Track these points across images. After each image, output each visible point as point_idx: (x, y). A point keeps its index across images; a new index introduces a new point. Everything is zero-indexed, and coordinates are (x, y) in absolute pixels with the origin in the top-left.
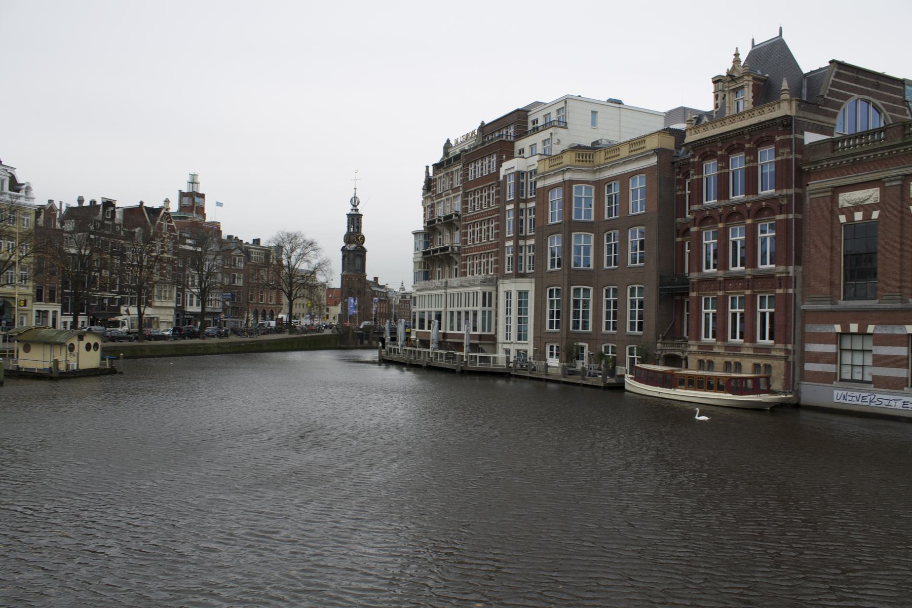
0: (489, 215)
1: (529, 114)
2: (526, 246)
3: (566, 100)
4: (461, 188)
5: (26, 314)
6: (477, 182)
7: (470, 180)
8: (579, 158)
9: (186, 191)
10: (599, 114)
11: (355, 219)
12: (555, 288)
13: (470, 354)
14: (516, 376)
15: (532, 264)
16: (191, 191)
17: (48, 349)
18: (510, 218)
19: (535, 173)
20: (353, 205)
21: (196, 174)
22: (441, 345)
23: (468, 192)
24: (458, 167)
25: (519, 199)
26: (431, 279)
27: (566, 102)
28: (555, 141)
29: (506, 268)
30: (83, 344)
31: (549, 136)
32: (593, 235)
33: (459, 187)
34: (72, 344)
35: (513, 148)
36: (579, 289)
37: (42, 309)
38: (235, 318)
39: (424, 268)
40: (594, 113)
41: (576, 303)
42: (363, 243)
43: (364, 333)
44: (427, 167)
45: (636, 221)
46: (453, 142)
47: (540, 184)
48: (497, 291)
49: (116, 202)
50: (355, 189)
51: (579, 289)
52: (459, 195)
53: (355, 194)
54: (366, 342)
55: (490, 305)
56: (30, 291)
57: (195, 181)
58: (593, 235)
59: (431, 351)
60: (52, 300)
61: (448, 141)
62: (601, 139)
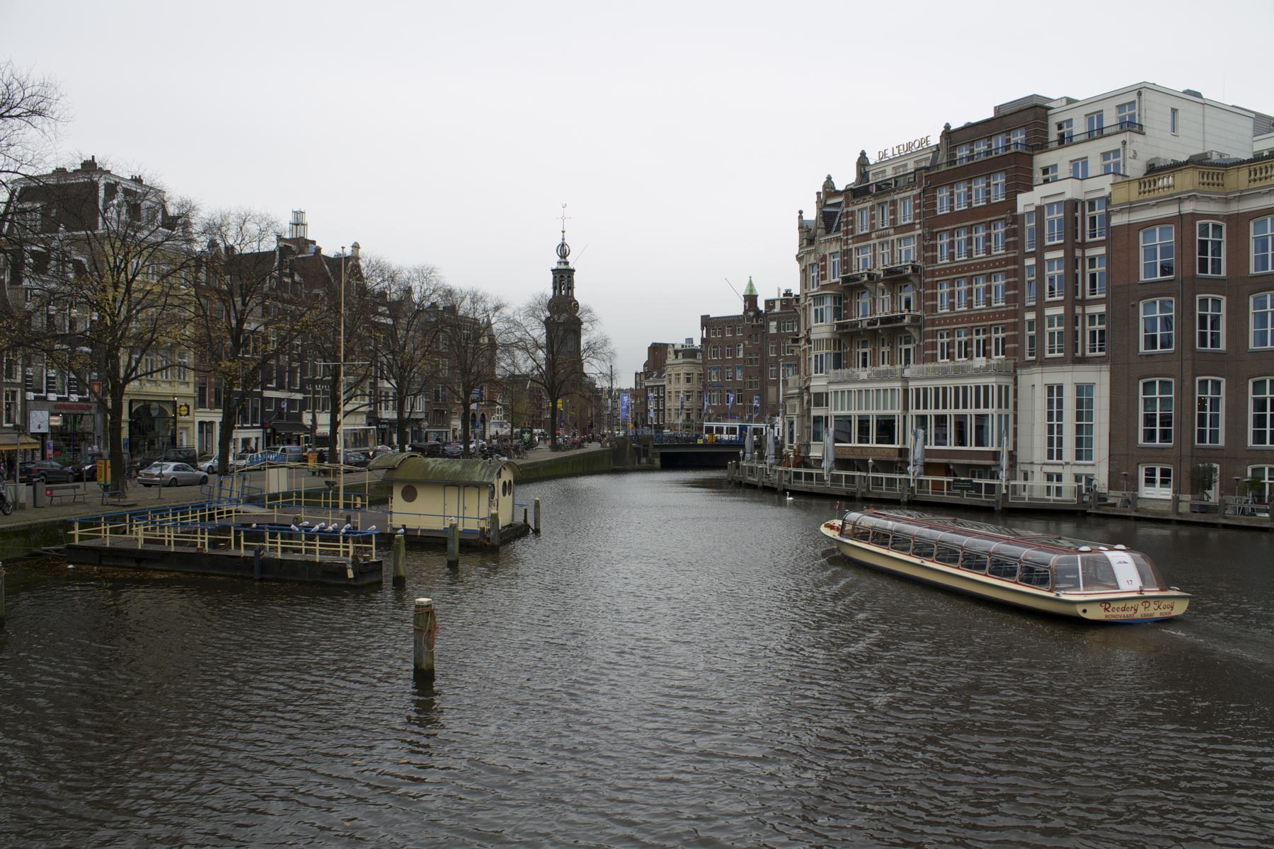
0: (972, 271)
1: (1050, 112)
3: (1140, 90)
4: (917, 226)
5: (186, 429)
6: (954, 217)
7: (939, 213)
10: (1180, 113)
11: (566, 276)
13: (836, 472)
14: (1098, 515)
17: (452, 497)
20: (561, 257)
22: (929, 468)
24: (908, 194)
25: (1073, 242)
26: (848, 366)
27: (1140, 94)
28: (1129, 154)
29: (1047, 348)
31: (1119, 146)
32: (1224, 298)
33: (914, 224)
35: (1031, 164)
36: (1206, 381)
37: (207, 420)
38: (440, 427)
39: (835, 349)
40: (1174, 111)
43: (641, 446)
46: (873, 158)
47: (1116, 221)
48: (1016, 383)
51: (1206, 381)
52: (913, 236)
54: (644, 460)
55: (1007, 407)
56: (190, 390)
57: (300, 221)
58: (1224, 298)
59: (911, 478)
61: (863, 154)
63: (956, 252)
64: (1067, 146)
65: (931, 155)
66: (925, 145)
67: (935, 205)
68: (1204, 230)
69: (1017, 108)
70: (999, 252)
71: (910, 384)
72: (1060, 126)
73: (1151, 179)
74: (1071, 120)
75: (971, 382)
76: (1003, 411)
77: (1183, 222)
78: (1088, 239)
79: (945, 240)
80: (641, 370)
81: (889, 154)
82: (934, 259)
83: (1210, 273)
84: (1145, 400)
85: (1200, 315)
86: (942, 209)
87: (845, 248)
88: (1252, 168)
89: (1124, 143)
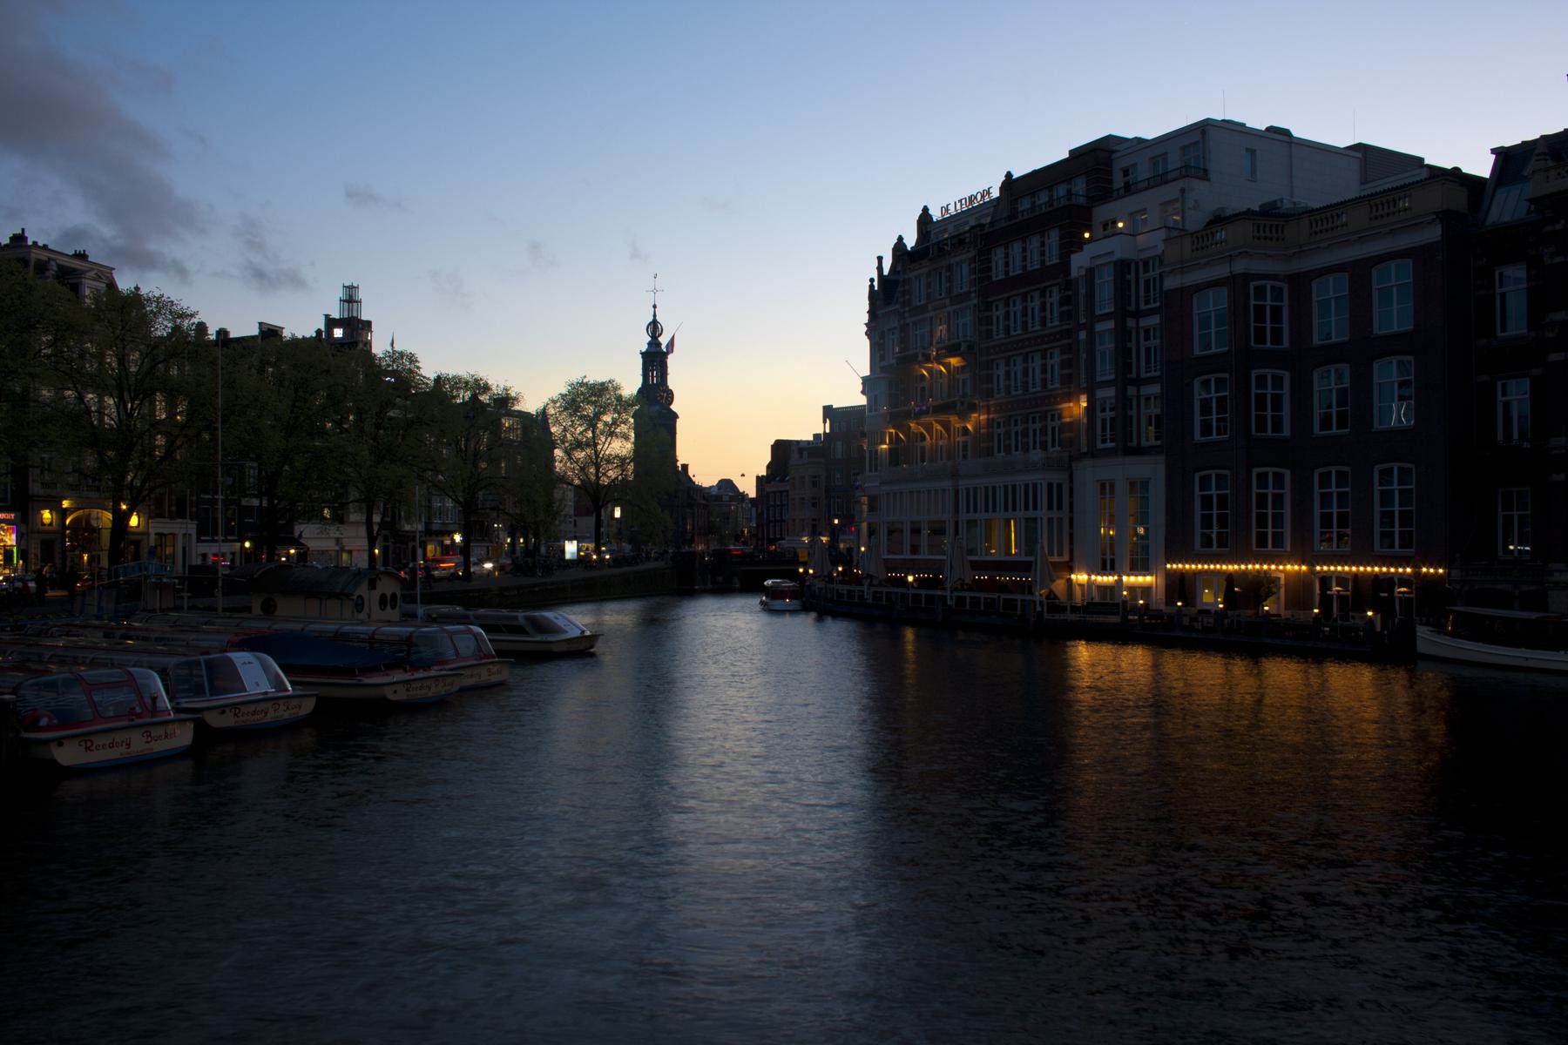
1: (1114, 156)
2: (1138, 328)
4: (973, 295)
6: (1011, 283)
7: (994, 279)
8: (1258, 232)
9: (337, 317)
12: (1213, 473)
15: (1108, 432)
16: (346, 316)
18: (1106, 346)
19: (1161, 262)
21: (355, 285)
23: (992, 302)
24: (964, 256)
25: (1125, 309)
27: (1204, 133)
30: (376, 595)
33: (970, 292)
34: (360, 597)
36: (1266, 474)
41: (1262, 499)
42: (671, 402)
44: (880, 259)
45: (1391, 345)
46: (936, 214)
47: (1169, 284)
48: (1071, 481)
49: (284, 331)
50: (655, 307)
53: (655, 316)
55: (1060, 507)
60: (180, 513)
61: (925, 209)
62: (1281, 200)
63: (1049, 316)
64: (1116, 200)
65: (992, 210)
66: (987, 199)
67: (990, 269)
68: (1260, 292)
69: (1202, 124)
70: (1055, 324)
71: (961, 482)
72: (1126, 172)
73: (1209, 232)
74: (1166, 153)
75: (1020, 479)
76: (1055, 514)
77: (1237, 283)
78: (1143, 307)
79: (1001, 312)
80: (763, 472)
81: (952, 211)
82: (989, 334)
83: (1268, 345)
84: (1322, 494)
85: (1256, 394)
86: (998, 273)
87: (902, 322)
88: (1372, 203)
89: (1183, 191)
